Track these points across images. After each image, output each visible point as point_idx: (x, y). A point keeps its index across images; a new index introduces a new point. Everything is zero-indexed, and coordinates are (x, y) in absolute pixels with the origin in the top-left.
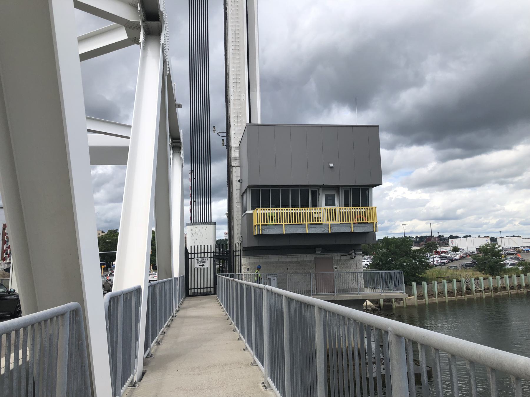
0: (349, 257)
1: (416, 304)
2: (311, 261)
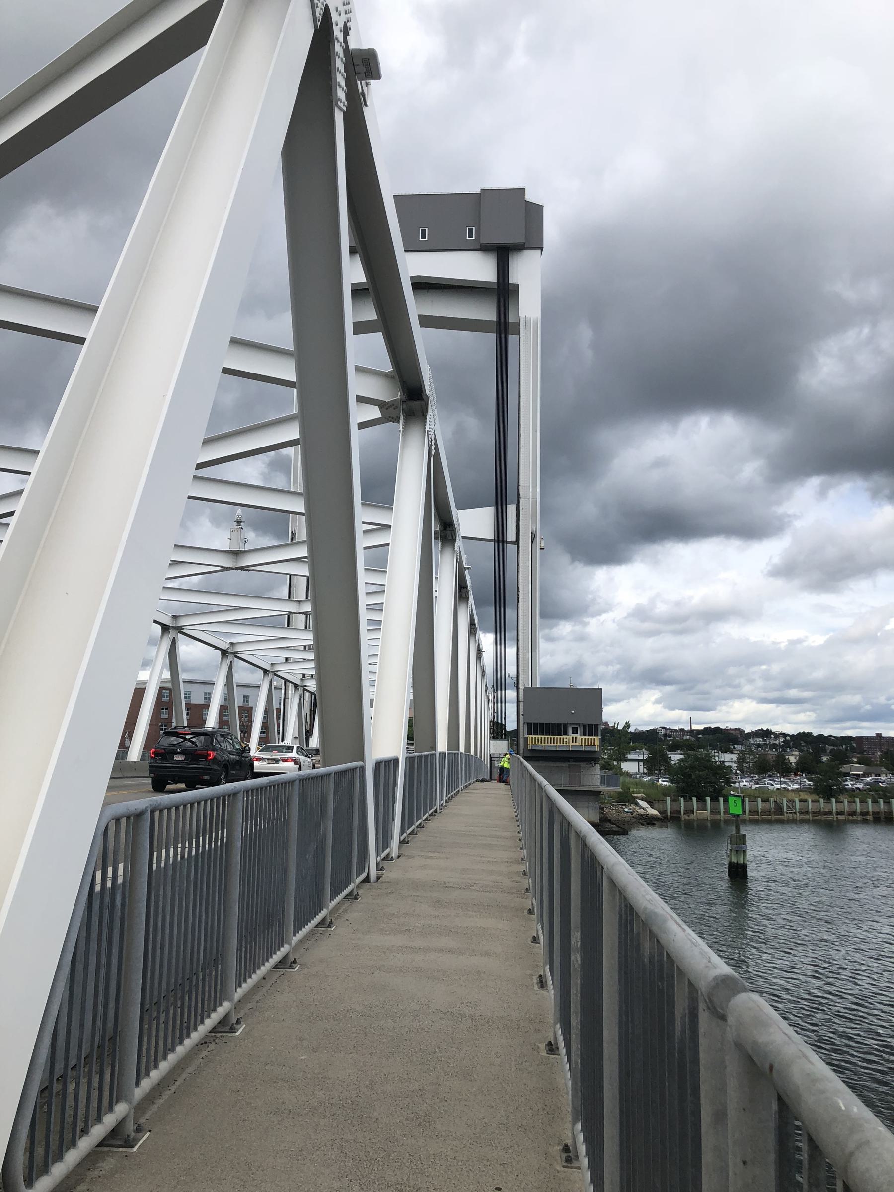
0: (591, 765)
1: (709, 819)
2: (566, 767)
